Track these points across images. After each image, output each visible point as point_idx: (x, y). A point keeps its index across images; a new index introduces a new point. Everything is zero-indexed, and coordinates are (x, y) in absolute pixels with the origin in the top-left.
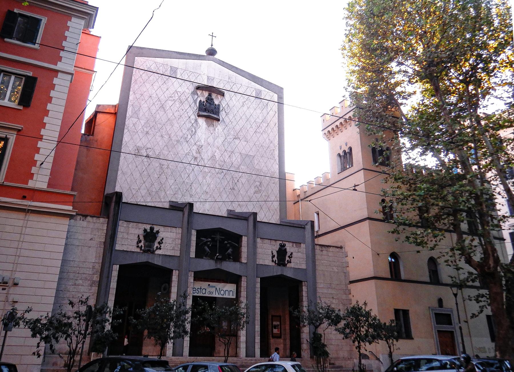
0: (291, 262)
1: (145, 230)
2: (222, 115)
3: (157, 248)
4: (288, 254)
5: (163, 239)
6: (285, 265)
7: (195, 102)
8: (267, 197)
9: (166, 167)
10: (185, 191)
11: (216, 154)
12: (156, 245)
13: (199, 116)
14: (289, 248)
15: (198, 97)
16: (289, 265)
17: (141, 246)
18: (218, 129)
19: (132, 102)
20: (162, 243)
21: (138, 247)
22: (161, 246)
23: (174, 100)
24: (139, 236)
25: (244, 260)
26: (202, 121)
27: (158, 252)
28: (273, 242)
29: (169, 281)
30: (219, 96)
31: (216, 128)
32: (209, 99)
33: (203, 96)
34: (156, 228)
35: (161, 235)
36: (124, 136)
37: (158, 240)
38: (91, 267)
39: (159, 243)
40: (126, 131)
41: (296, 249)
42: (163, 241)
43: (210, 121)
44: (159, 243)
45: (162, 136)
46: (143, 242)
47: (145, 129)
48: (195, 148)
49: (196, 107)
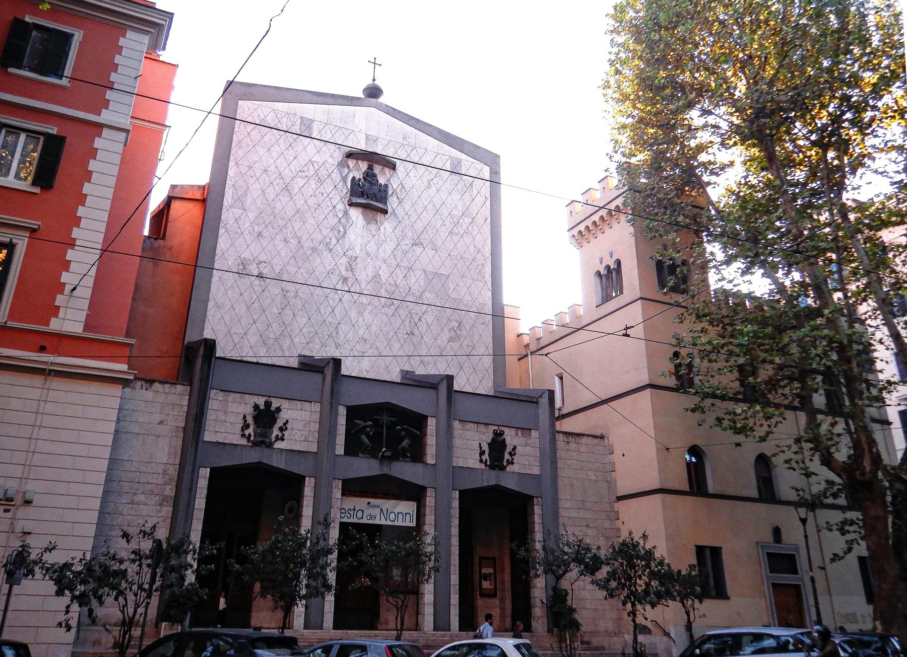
0: (513, 463)
1: (256, 407)
2: (392, 203)
3: (277, 438)
4: (509, 449)
5: (287, 421)
6: (503, 468)
7: (344, 179)
8: (471, 348)
9: (293, 295)
10: (327, 337)
11: (381, 272)
12: (276, 432)
13: (351, 204)
14: (511, 438)
15: (349, 172)
16: (509, 468)
17: (250, 434)
18: (385, 229)
19: (233, 180)
20: (286, 429)
21: (243, 435)
22: (284, 435)
23: (306, 176)
24: (245, 417)
25: (430, 459)
26: (356, 214)
27: (279, 445)
28: (482, 428)
29: (298, 497)
30: (387, 170)
31: (381, 226)
32: (370, 176)
33: (358, 170)
34: (275, 404)
35: (284, 416)
36: (220, 240)
37: (280, 423)
38: (161, 471)
39: (281, 429)
40: (222, 231)
41: (523, 440)
42: (288, 426)
43: (370, 213)
44: (281, 429)
45: (286, 240)
46: (252, 427)
47: (256, 228)
48: (344, 261)
49: (345, 189)
